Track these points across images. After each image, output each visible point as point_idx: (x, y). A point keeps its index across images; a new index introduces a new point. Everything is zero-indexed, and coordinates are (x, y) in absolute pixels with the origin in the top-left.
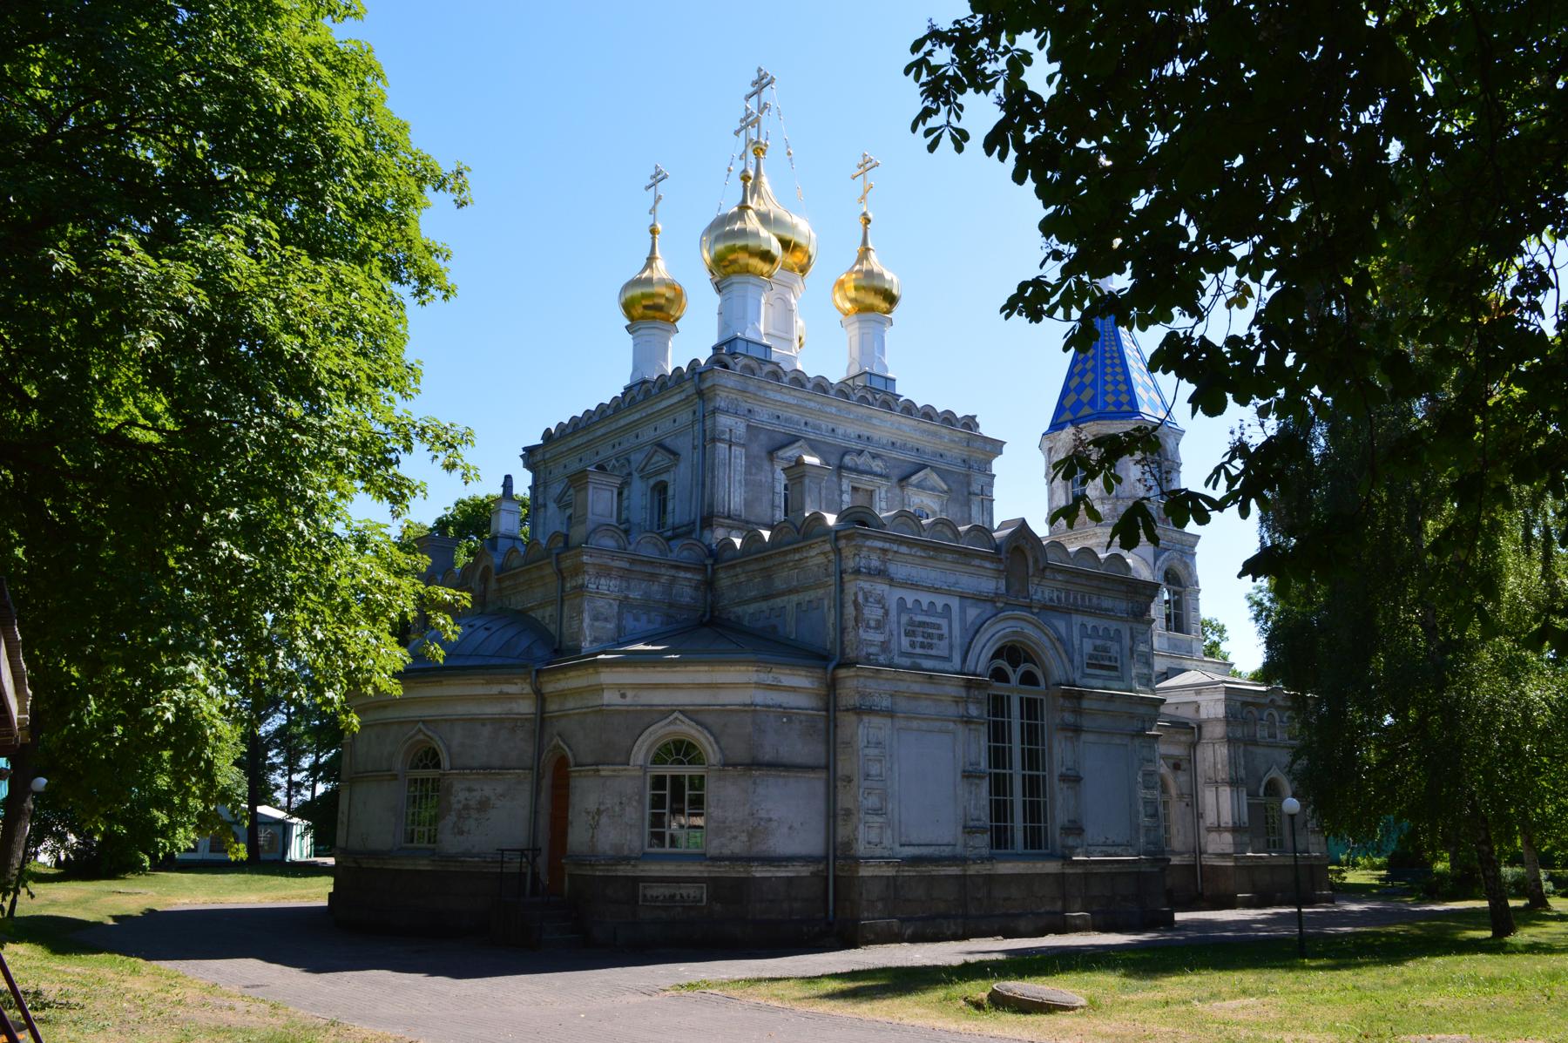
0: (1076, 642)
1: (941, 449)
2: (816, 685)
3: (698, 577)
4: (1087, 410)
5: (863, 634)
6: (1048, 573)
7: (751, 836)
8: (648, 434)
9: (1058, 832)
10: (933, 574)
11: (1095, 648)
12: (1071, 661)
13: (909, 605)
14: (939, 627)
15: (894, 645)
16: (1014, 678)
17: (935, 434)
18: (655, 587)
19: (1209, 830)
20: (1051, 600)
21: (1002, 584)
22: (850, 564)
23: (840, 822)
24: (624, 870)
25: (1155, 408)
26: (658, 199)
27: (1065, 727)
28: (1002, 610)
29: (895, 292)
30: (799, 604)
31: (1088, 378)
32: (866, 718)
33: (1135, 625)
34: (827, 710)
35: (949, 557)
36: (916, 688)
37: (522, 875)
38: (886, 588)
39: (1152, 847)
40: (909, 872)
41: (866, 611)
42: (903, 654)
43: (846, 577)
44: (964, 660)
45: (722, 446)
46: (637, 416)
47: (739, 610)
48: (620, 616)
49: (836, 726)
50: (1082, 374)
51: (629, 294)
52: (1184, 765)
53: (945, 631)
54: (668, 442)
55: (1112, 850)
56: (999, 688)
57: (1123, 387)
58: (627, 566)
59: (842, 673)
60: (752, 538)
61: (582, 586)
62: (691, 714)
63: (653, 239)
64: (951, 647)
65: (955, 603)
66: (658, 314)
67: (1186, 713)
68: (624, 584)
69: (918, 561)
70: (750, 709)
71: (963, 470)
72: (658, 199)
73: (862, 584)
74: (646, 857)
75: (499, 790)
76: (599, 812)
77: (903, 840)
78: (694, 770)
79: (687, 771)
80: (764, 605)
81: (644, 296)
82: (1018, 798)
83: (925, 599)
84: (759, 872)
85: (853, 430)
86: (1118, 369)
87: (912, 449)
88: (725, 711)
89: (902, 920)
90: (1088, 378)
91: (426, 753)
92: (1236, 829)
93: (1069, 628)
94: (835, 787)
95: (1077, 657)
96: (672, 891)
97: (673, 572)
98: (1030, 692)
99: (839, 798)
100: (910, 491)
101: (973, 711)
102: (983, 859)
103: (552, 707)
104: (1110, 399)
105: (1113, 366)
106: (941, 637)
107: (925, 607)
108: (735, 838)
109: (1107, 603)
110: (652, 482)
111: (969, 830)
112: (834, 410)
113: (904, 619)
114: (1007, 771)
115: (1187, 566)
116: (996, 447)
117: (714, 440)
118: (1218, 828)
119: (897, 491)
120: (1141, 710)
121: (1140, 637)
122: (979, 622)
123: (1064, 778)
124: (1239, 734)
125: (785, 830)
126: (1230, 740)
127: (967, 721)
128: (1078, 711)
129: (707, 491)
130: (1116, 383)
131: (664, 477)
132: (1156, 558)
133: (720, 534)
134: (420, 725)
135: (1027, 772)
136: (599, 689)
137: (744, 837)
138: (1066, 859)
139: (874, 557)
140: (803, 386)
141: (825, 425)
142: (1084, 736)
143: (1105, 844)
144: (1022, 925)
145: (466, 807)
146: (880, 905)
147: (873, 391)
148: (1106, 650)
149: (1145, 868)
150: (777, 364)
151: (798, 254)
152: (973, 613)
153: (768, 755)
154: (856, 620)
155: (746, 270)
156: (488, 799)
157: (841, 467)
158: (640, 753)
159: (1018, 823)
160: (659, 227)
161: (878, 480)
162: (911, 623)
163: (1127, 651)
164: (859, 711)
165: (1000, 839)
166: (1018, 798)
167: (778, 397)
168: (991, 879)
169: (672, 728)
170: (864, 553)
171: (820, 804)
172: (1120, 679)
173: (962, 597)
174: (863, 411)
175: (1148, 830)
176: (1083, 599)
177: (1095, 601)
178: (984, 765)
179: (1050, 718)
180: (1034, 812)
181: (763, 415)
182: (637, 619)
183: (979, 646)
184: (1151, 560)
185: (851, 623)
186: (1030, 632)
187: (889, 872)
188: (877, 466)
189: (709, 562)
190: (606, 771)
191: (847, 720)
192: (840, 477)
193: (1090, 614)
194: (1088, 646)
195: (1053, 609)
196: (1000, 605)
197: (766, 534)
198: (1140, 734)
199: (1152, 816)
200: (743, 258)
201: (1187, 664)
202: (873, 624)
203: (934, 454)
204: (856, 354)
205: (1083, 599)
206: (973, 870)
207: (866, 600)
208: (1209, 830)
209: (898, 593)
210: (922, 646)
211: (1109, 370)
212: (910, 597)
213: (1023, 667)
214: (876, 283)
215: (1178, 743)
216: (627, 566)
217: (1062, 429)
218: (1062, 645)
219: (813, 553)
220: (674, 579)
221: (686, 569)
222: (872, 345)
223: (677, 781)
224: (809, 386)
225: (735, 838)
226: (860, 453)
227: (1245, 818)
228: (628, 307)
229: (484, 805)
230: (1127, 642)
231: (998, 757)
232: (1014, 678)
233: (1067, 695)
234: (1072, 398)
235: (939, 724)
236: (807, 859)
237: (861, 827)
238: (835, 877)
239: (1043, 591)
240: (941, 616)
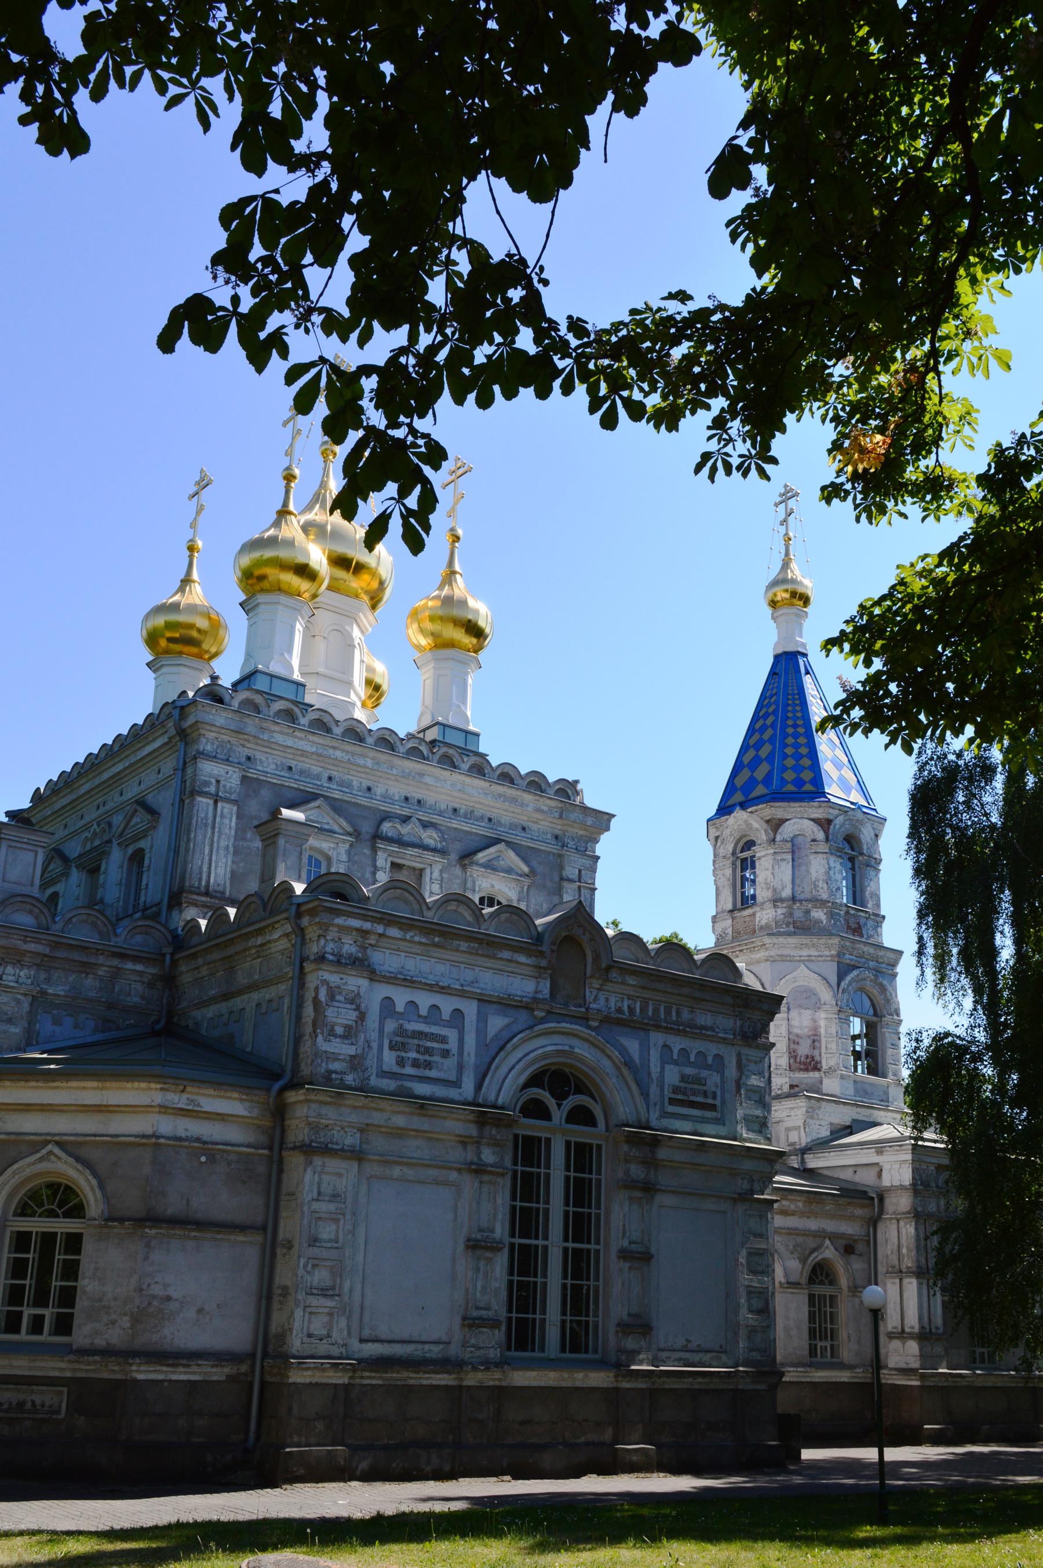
0: (655, 1069)
1: (523, 819)
2: (256, 1112)
3: (152, 970)
4: (760, 790)
5: (322, 1044)
6: (614, 974)
7: (135, 1320)
8: (132, 791)
9: (612, 1329)
10: (440, 968)
11: (684, 1078)
12: (645, 1095)
13: (400, 1007)
14: (443, 1040)
15: (371, 1061)
16: (558, 1115)
17: (514, 800)
18: (89, 981)
19: (891, 1336)
20: (619, 1010)
21: (545, 987)
22: (314, 949)
23: (275, 1306)
25: (847, 789)
26: (200, 509)
27: (629, 1184)
28: (542, 1021)
29: (481, 623)
30: (258, 1005)
31: (764, 752)
32: (318, 1161)
33: (745, 1050)
34: (270, 1148)
35: (464, 946)
36: (400, 1121)
38: (364, 983)
39: (755, 1355)
40: (371, 1379)
41: (330, 1013)
43: (308, 967)
44: (479, 1087)
45: (204, 803)
46: (119, 767)
47: (197, 1014)
48: (32, 1017)
49: (281, 1171)
50: (758, 746)
51: (150, 625)
52: (860, 1247)
53: (453, 1045)
54: (150, 799)
55: (696, 1357)
56: (532, 1127)
57: (806, 762)
58: (47, 951)
59: (292, 1096)
60: (218, 918)
61: (674, 1092)
62: (69, 1146)
63: (191, 557)
64: (460, 1068)
65: (470, 1009)
66: (187, 649)
67: (866, 1178)
68: (43, 976)
69: (417, 949)
70: (152, 1141)
71: (554, 848)
72: (200, 509)
73: (326, 976)
77: (366, 1333)
79: (62, 1226)
80: (223, 1007)
81: (169, 626)
82: (554, 1280)
83: (425, 1001)
84: (143, 1373)
85: (398, 790)
86: (802, 740)
87: (482, 818)
88: (116, 1144)
89: (354, 1449)
90: (764, 752)
92: (924, 1336)
93: (645, 1049)
94: (273, 1255)
95: (654, 1090)
97: (115, 962)
98: (581, 1134)
99: (278, 1271)
100: (475, 871)
101: (488, 1156)
102: (488, 1365)
104: (789, 776)
105: (796, 736)
106: (446, 1054)
107: (424, 1011)
108: (113, 1322)
109: (704, 1019)
110: (130, 850)
111: (471, 1323)
112: (369, 763)
113: (390, 1026)
114: (540, 1242)
115: (883, 989)
116: (602, 821)
117: (194, 793)
118: (902, 1335)
119: (458, 871)
120: (748, 1165)
121: (752, 1067)
123: (625, 1255)
124: (932, 1207)
125: (192, 1314)
126: (918, 1216)
127: (478, 1170)
128: (651, 1163)
129: (181, 858)
130: (798, 757)
131: (142, 844)
132: (840, 978)
133: (190, 913)
135: (570, 1245)
137: (125, 1322)
138: (620, 1367)
139: (348, 940)
140: (328, 730)
141: (358, 781)
142: (659, 1198)
143: (685, 1349)
144: (547, 1460)
146: (320, 1426)
147: (449, 747)
148: (700, 1081)
149: (745, 1385)
150: (483, 756)
151: (365, 577)
152: (496, 1023)
153: (173, 1206)
154: (314, 1024)
155: (279, 589)
157: (377, 836)
159: (553, 1314)
160: (200, 544)
161: (429, 856)
162: (401, 1032)
163: (731, 1086)
164: (309, 1150)
165: (522, 1336)
166: (554, 1280)
167: (290, 742)
168: (501, 1393)
169: (44, 1166)
170: (333, 934)
171: (250, 1279)
172: (720, 1121)
173: (483, 1000)
174: (412, 766)
175: (752, 1331)
176: (668, 1011)
177: (686, 1015)
178: (500, 1230)
179: (609, 1172)
180: (577, 1301)
181: (268, 764)
182: (57, 1022)
183: (504, 1069)
184: (834, 979)
185: (309, 1029)
186: (585, 1052)
187: (340, 1378)
188: (430, 837)
189: (168, 950)
191: (294, 1161)
192: (374, 850)
193: (678, 1032)
194: (672, 1076)
195: (621, 1023)
196: (540, 1014)
197: (232, 912)
198: (745, 1197)
199: (759, 1312)
200: (272, 573)
201: (879, 1115)
202: (339, 1030)
203: (513, 826)
204: (429, 702)
205: (668, 1011)
206: (472, 1379)
207: (332, 997)
208: (891, 1336)
209: (385, 990)
210: (415, 1064)
211: (790, 740)
212: (401, 997)
213: (572, 1101)
214: (456, 612)
215: (851, 1218)
216: (47, 951)
217: (730, 813)
218: (633, 1074)
219: (275, 936)
220: (116, 973)
221: (135, 959)
222: (449, 690)
223: (48, 1238)
224: (338, 731)
225: (113, 1322)
226: (405, 820)
227: (939, 1321)
228: (152, 640)
230: (731, 1072)
231: (526, 1221)
232: (558, 1115)
233: (634, 1140)
234: (745, 774)
235: (432, 1173)
236: (219, 1357)
237: (298, 1313)
238: (263, 1383)
239: (605, 999)
240: (449, 1024)
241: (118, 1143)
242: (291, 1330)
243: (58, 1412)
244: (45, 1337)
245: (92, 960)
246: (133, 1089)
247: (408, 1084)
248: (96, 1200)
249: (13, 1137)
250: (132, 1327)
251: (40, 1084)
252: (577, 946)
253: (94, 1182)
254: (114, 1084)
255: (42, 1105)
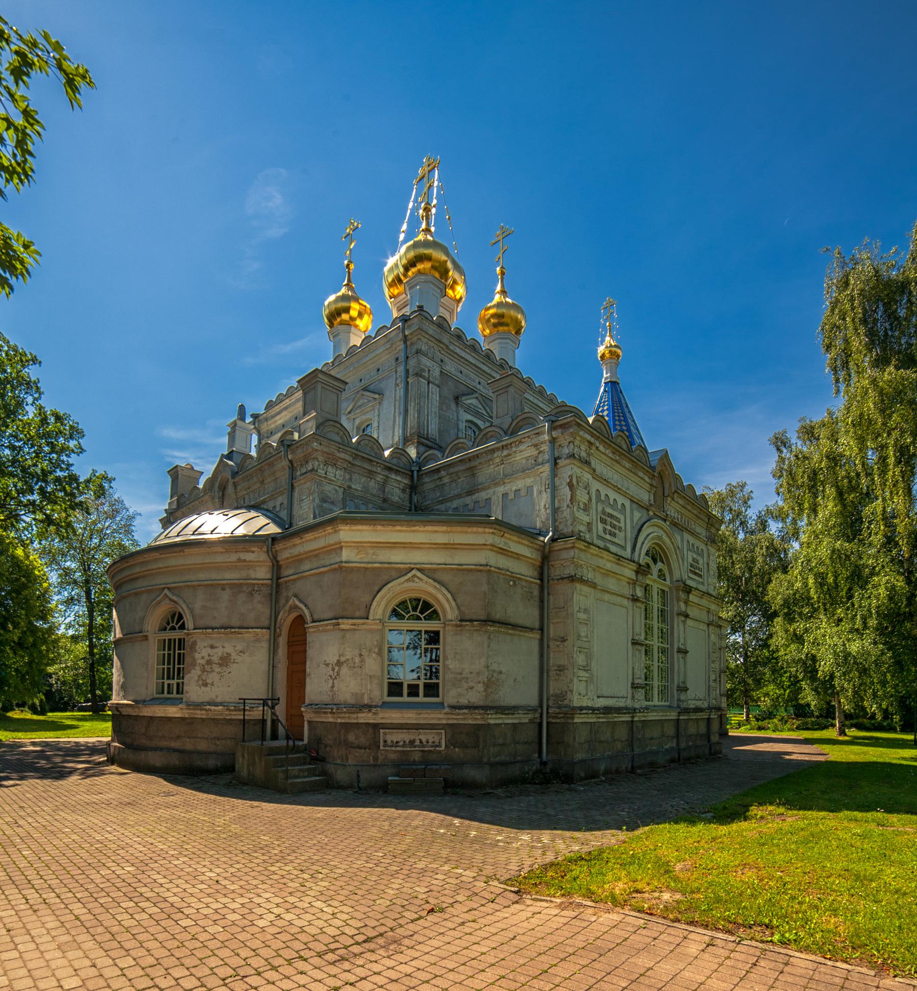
7: (487, 686)
18: (372, 484)
24: (365, 717)
36: (609, 566)
37: (263, 721)
42: (599, 537)
58: (351, 459)
62: (429, 572)
68: (348, 477)
69: (609, 462)
74: (385, 705)
75: (239, 647)
76: (339, 663)
77: (600, 693)
78: (432, 625)
83: (613, 495)
84: (493, 719)
91: (173, 616)
96: (412, 737)
97: (386, 473)
103: (286, 572)
105: (620, 421)
122: (640, 524)
134: (166, 591)
136: (338, 548)
137: (480, 687)
145: (209, 662)
156: (229, 655)
158: (381, 606)
190: (345, 624)
213: (660, 565)
216: (351, 459)
221: (397, 472)
225: (472, 688)
229: (225, 661)
236: (528, 709)
237: (575, 680)
238: (548, 723)
241: (461, 570)
242: (571, 691)
243: (440, 746)
244: (421, 699)
245: (374, 469)
246: (471, 533)
247: (608, 545)
248: (451, 608)
249: (386, 565)
250: (485, 690)
251: (404, 528)
252: (341, 569)
253: (449, 596)
254: (459, 529)
255: (404, 543)
